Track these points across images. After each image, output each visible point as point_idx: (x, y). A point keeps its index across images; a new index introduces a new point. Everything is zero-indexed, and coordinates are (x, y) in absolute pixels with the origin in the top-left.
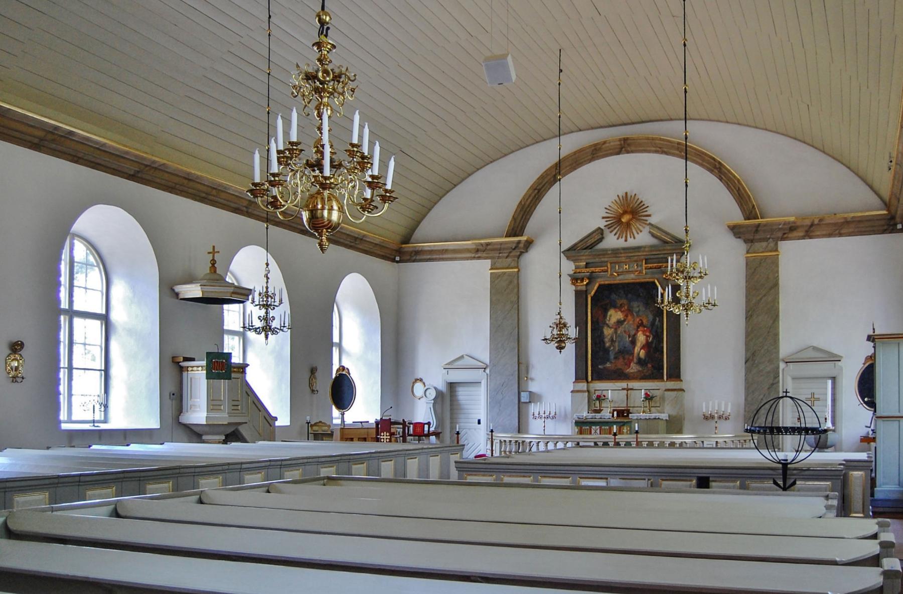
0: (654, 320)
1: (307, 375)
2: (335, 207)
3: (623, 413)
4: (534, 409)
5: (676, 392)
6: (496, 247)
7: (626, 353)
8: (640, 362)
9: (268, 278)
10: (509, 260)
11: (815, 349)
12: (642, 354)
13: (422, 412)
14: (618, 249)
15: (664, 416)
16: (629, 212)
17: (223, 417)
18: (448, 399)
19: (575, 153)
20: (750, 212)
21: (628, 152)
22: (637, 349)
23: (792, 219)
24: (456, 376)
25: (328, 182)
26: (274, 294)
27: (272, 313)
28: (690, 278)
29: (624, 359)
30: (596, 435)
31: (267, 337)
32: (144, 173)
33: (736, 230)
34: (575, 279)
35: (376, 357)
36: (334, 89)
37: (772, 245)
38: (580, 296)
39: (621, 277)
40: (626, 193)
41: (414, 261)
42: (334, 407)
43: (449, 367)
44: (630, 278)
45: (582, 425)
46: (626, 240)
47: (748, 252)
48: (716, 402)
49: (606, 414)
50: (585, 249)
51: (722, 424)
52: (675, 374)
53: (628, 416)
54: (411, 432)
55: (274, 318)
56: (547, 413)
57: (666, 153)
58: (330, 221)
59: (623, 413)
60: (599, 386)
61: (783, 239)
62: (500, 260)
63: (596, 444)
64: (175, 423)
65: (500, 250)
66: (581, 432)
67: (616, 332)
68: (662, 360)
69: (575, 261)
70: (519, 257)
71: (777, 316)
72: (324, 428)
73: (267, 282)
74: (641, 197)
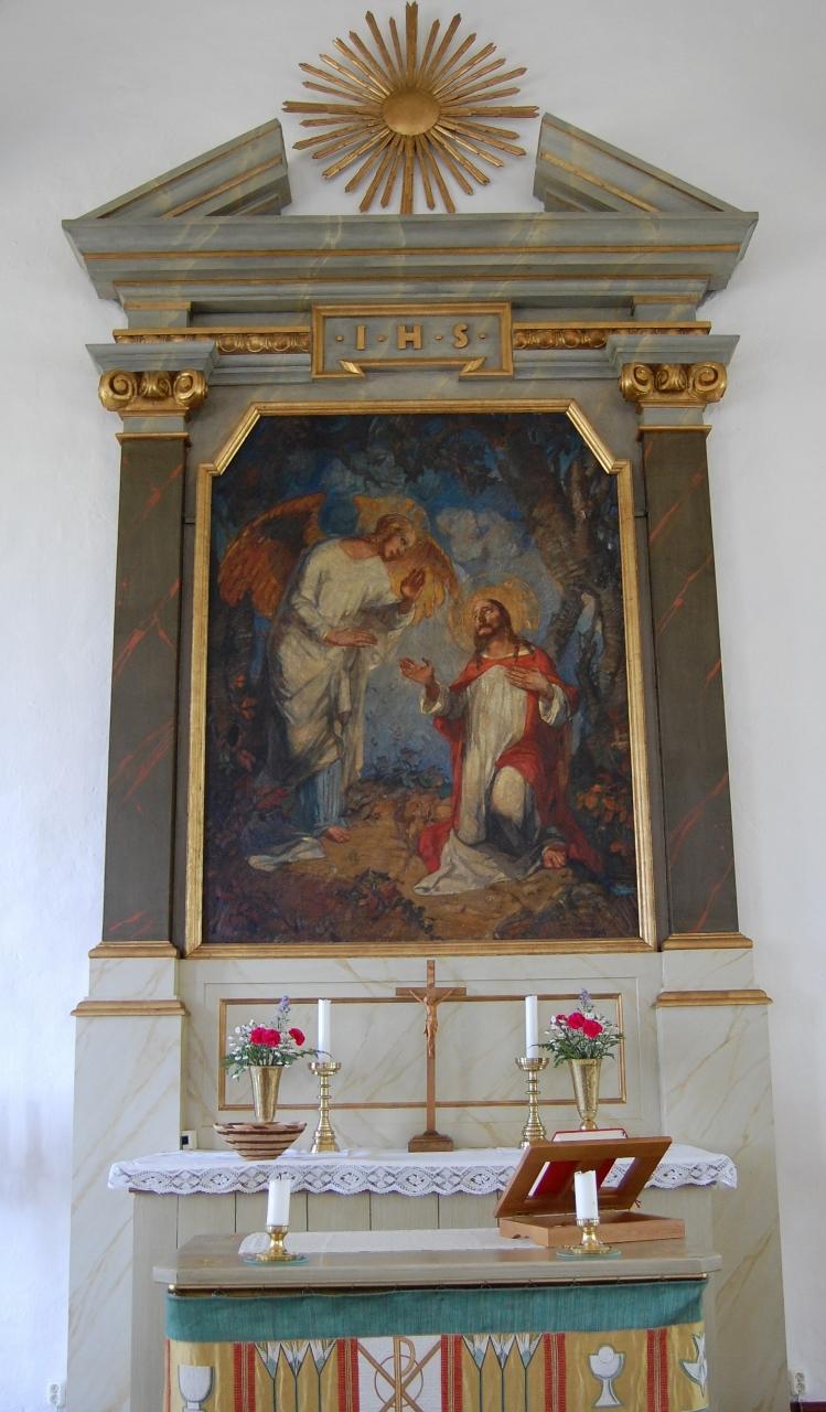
7: (410, 784)
8: (496, 834)
12: (511, 790)
22: (477, 764)
29: (402, 819)
67: (353, 669)
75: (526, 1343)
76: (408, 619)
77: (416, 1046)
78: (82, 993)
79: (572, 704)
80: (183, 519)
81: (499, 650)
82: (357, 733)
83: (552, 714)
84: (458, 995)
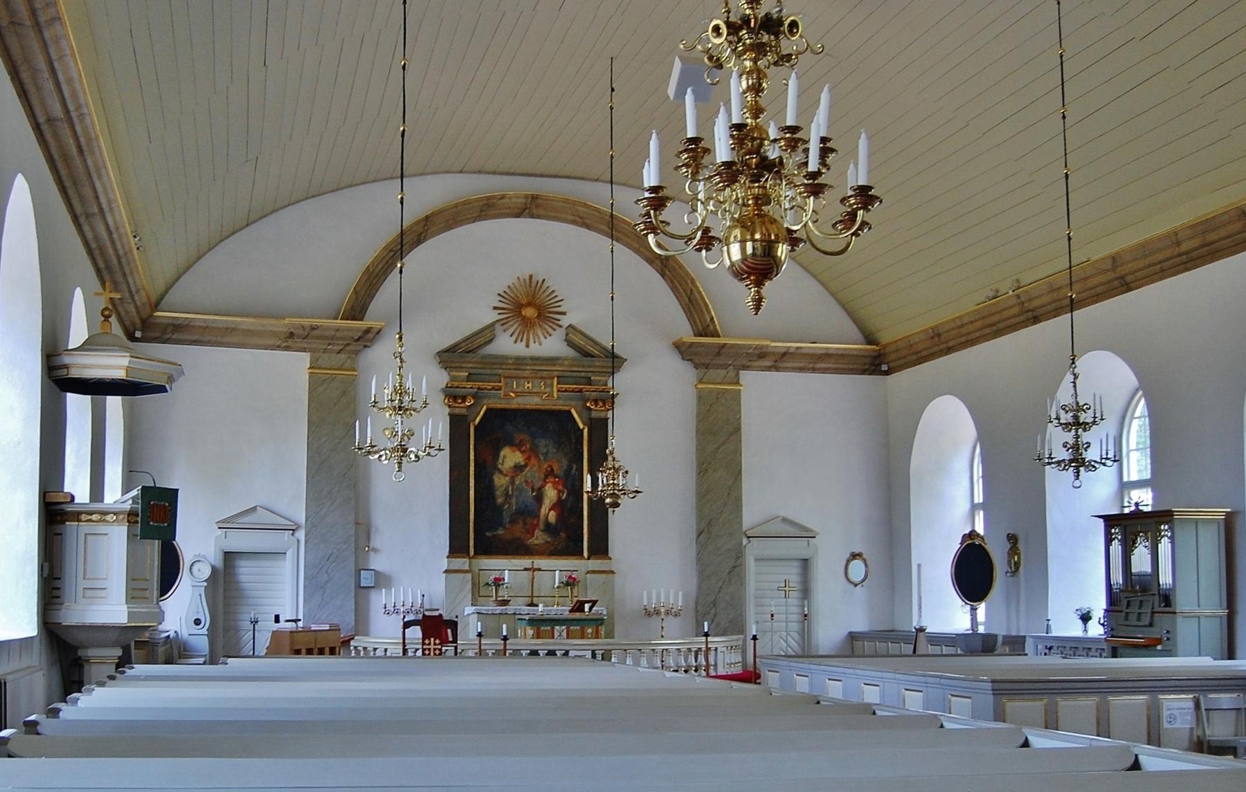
0: (570, 467)
4: (379, 599)
5: (604, 576)
6: (326, 333)
7: (528, 513)
8: (549, 528)
10: (343, 356)
11: (785, 520)
12: (552, 517)
14: (524, 358)
16: (530, 306)
19: (456, 206)
21: (532, 216)
22: (544, 510)
24: (239, 541)
27: (1085, 437)
29: (525, 524)
33: (683, 350)
37: (732, 374)
38: (458, 425)
39: (520, 400)
43: (226, 525)
44: (533, 402)
46: (527, 346)
48: (662, 591)
52: (600, 548)
55: (1089, 444)
56: (408, 606)
57: (588, 227)
61: (746, 368)
62: (326, 355)
63: (594, 656)
65: (331, 339)
67: (512, 482)
68: (581, 530)
70: (357, 353)
77: (527, 583)
81: (551, 479)
82: (514, 500)
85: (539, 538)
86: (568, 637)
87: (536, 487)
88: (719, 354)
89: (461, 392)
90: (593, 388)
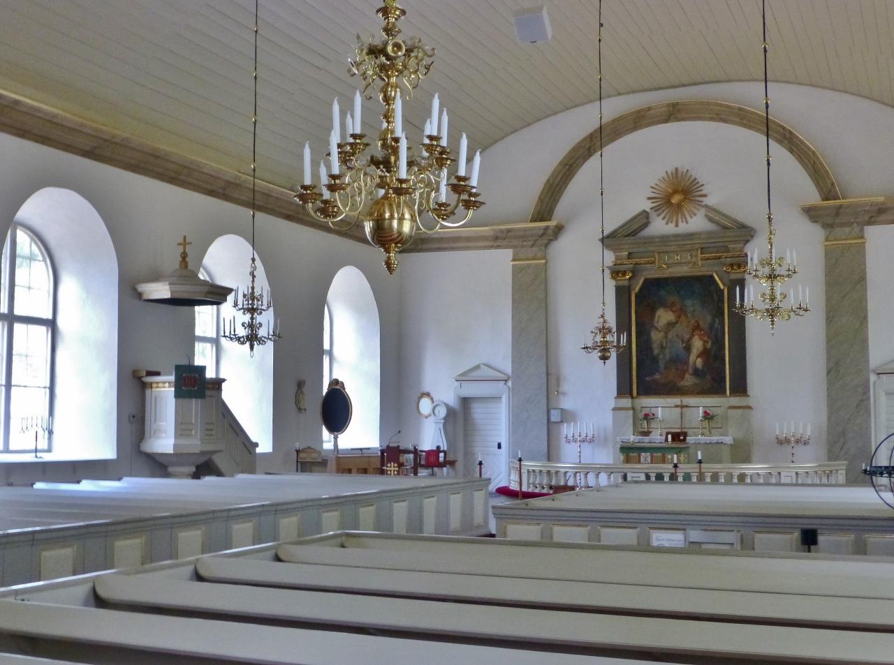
1: (293, 389)
2: (407, 216)
3: (679, 437)
4: (567, 430)
7: (679, 362)
8: (696, 372)
9: (254, 277)
10: (535, 249)
13: (430, 437)
15: (728, 440)
16: (680, 192)
17: (195, 444)
18: (460, 417)
20: (828, 192)
22: (692, 357)
23: (881, 199)
24: (470, 390)
25: (404, 186)
26: (261, 296)
27: (259, 319)
28: (775, 277)
30: (646, 464)
31: (252, 348)
32: (102, 149)
33: (811, 213)
34: (615, 273)
35: (374, 367)
36: (405, 66)
40: (677, 169)
41: (420, 251)
42: (324, 427)
43: (462, 378)
45: (629, 452)
46: (677, 226)
47: (827, 240)
49: (657, 437)
50: (624, 237)
51: (800, 450)
52: (740, 387)
53: (685, 440)
54: (423, 462)
55: (261, 325)
56: (583, 435)
57: (725, 121)
58: (400, 233)
59: (679, 437)
60: (649, 402)
61: (870, 223)
63: (648, 477)
64: (134, 452)
66: (627, 461)
67: (666, 337)
68: (723, 372)
69: (614, 250)
70: (546, 246)
71: (865, 317)
72: (313, 455)
73: (253, 281)
74: (695, 173)
75: (660, 454)
76: (678, 326)
78: (613, 406)
79: (713, 343)
80: (548, 420)
81: (698, 332)
82: (667, 351)
83: (709, 346)
84: (687, 406)
85: (689, 380)
86: (652, 462)
87: (685, 340)
88: (837, 214)
89: (622, 268)
90: (730, 254)
